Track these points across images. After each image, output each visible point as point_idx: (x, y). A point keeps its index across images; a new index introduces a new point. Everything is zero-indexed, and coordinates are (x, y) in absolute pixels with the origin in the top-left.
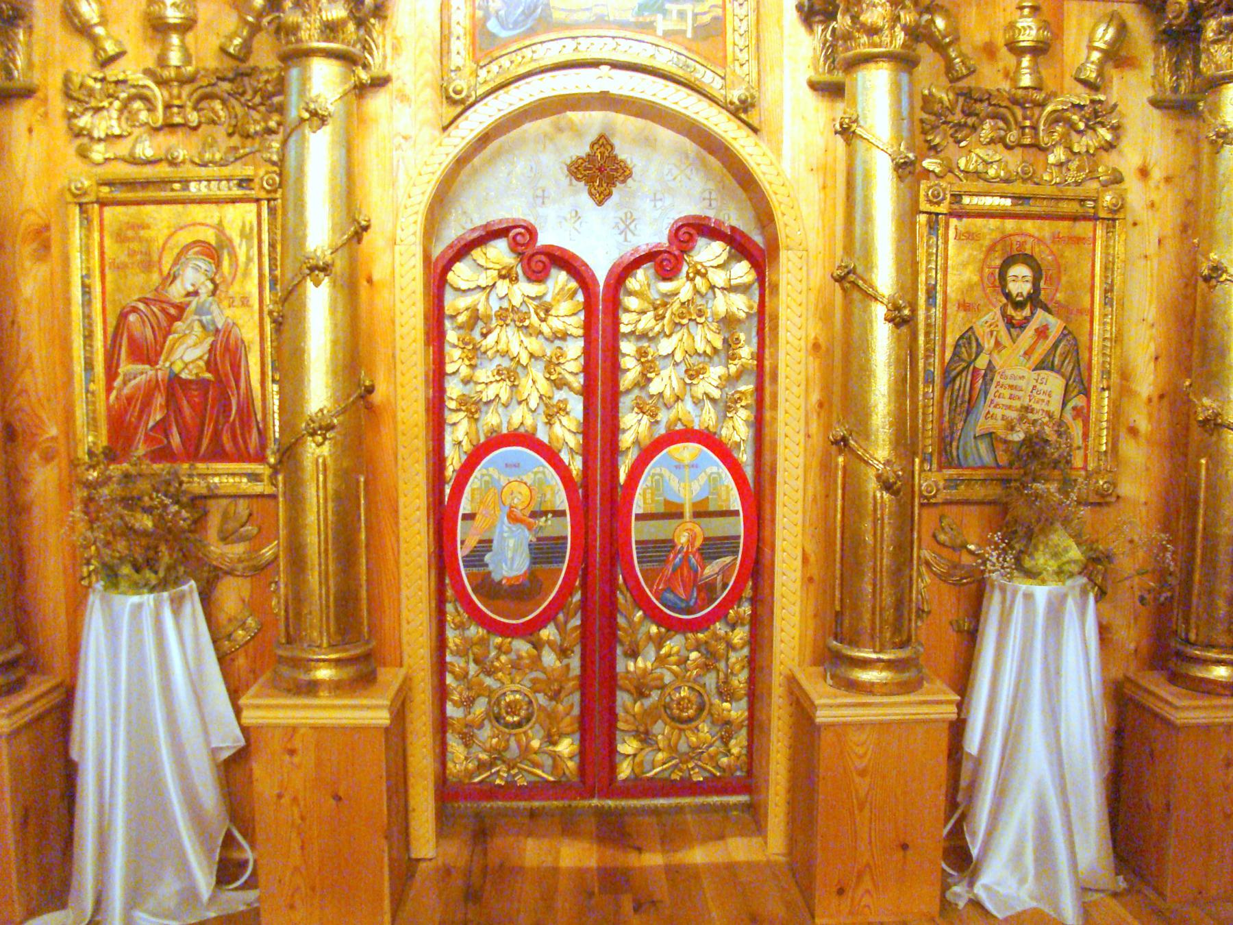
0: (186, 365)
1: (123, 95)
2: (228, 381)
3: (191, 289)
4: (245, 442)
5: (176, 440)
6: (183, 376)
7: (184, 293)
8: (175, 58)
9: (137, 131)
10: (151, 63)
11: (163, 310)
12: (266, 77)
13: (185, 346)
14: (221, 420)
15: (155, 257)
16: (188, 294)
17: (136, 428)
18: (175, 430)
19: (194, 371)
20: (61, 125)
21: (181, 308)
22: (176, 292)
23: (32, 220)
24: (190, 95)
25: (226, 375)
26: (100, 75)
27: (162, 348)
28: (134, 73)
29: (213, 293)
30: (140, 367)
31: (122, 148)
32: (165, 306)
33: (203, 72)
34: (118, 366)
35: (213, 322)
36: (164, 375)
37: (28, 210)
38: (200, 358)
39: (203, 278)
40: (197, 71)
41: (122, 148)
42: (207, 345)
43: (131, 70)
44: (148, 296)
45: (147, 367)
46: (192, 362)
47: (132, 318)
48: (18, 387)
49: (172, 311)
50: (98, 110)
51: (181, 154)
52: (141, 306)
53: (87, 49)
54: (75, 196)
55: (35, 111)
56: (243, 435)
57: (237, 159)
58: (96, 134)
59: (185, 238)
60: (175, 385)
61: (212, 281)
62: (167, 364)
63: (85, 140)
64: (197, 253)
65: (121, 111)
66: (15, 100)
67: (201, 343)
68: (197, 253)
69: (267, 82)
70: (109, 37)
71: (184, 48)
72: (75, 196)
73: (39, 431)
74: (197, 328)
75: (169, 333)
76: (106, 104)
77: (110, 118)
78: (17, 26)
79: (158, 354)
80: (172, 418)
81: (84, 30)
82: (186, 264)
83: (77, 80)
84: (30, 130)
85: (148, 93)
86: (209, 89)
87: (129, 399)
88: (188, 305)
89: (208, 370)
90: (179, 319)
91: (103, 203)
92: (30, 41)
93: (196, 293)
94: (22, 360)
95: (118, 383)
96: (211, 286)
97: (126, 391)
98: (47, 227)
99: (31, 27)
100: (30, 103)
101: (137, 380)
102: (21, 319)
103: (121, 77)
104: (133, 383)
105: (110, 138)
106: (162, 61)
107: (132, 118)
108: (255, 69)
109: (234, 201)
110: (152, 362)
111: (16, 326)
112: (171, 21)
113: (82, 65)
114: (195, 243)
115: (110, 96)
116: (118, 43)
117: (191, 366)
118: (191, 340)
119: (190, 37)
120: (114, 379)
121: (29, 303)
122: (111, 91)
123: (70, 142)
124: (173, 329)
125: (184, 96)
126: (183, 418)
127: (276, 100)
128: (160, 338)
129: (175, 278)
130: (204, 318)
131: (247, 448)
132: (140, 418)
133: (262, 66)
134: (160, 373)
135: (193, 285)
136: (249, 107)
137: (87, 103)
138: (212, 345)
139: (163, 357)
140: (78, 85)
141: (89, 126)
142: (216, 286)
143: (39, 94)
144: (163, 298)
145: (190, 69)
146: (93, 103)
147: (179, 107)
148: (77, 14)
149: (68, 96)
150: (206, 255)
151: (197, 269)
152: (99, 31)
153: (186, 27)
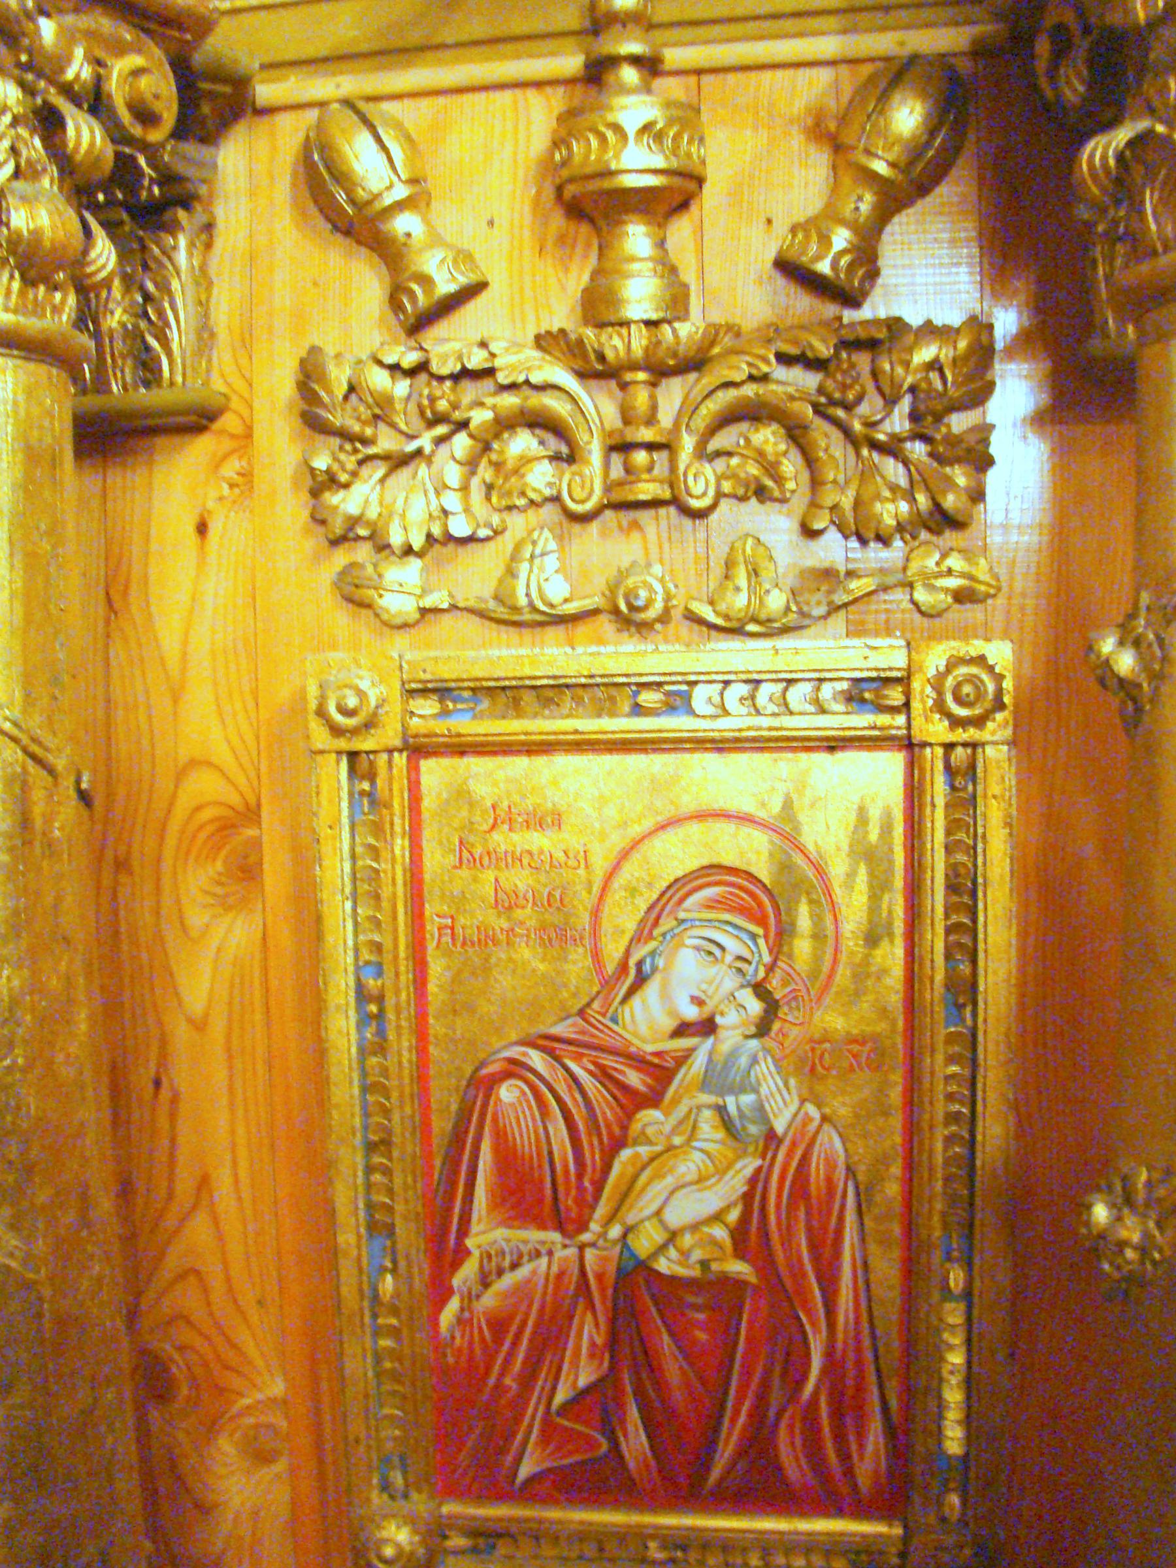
0: (673, 1236)
1: (480, 417)
2: (802, 1290)
3: (691, 1013)
4: (845, 1457)
5: (636, 1442)
6: (663, 1266)
7: (669, 1024)
8: (640, 296)
9: (517, 524)
10: (561, 314)
11: (604, 1075)
12: (925, 354)
13: (669, 1181)
14: (776, 1398)
15: (582, 903)
16: (682, 1029)
17: (519, 1405)
18: (633, 1414)
19: (697, 1255)
20: (292, 509)
21: (662, 1072)
22: (646, 1020)
23: (204, 786)
24: (689, 409)
25: (798, 1273)
26: (410, 359)
27: (599, 1186)
28: (515, 345)
29: (763, 1029)
30: (535, 1236)
31: (475, 577)
32: (608, 1061)
33: (727, 341)
34: (463, 1232)
35: (760, 1108)
36: (603, 1260)
37: (193, 763)
38: (717, 1217)
39: (730, 982)
40: (713, 334)
41: (475, 577)
42: (736, 1182)
43: (502, 332)
44: (558, 1030)
45: (556, 1236)
46: (695, 1227)
47: (507, 1093)
48: (172, 1262)
49: (634, 1078)
50: (399, 461)
51: (652, 589)
52: (536, 1059)
53: (367, 284)
54: (337, 731)
55: (217, 465)
56: (839, 1437)
57: (834, 609)
58: (396, 539)
59: (677, 854)
60: (636, 1290)
61: (760, 989)
62: (615, 1232)
63: (363, 553)
64: (712, 905)
65: (471, 465)
66: (161, 441)
67: (721, 1172)
68: (712, 905)
69: (934, 365)
70: (435, 240)
71: (668, 269)
72: (337, 731)
73: (236, 1382)
74: (709, 1129)
75: (618, 1144)
76: (425, 441)
77: (441, 487)
78: (173, 228)
79: (587, 1204)
80: (627, 1378)
81: (359, 226)
82: (675, 938)
83: (339, 377)
84: (202, 529)
85: (554, 403)
86: (750, 390)
87: (498, 1325)
88: (683, 1058)
89: (740, 1248)
90: (654, 1099)
91: (418, 749)
92: (203, 268)
93: (708, 1027)
94: (185, 1185)
95: (466, 1274)
96: (755, 1007)
97: (488, 1301)
98: (251, 813)
99: (209, 227)
100: (202, 447)
101: (524, 1271)
102: (181, 1075)
103: (477, 360)
104: (509, 1280)
105: (443, 542)
106: (599, 306)
107: (504, 490)
108: (895, 325)
109: (833, 745)
110: (569, 1224)
111: (165, 1094)
112: (631, 181)
113: (352, 321)
114: (713, 871)
115: (439, 419)
116: (464, 257)
117: (687, 1240)
118: (690, 1165)
119: (681, 230)
120: (456, 1264)
121: (200, 1026)
122: (442, 405)
123: (317, 559)
124: (635, 1127)
125: (666, 418)
126: (660, 1384)
127: (959, 422)
128: (593, 1156)
129: (641, 980)
130: (730, 1102)
131: (849, 1472)
132: (528, 1379)
133: (914, 319)
134: (590, 1254)
135: (698, 1001)
136: (875, 445)
137: (365, 442)
138: (753, 1181)
139: (601, 1211)
140: (341, 390)
141: (372, 514)
142: (772, 1007)
143: (229, 422)
144: (605, 1040)
145: (687, 331)
146: (387, 442)
147: (651, 447)
148: (343, 178)
149: (314, 423)
150: (743, 911)
151: (712, 951)
152: (404, 224)
153: (674, 197)
